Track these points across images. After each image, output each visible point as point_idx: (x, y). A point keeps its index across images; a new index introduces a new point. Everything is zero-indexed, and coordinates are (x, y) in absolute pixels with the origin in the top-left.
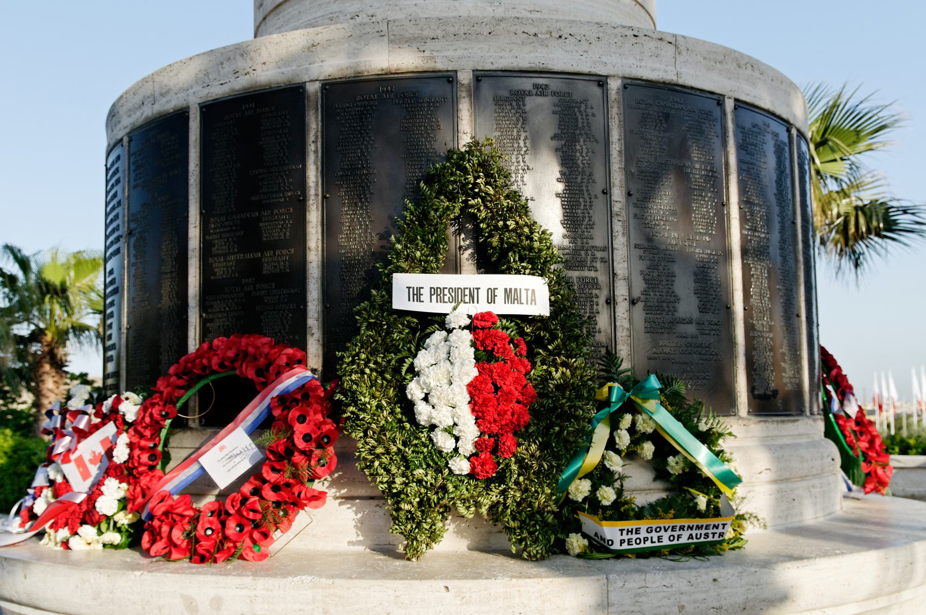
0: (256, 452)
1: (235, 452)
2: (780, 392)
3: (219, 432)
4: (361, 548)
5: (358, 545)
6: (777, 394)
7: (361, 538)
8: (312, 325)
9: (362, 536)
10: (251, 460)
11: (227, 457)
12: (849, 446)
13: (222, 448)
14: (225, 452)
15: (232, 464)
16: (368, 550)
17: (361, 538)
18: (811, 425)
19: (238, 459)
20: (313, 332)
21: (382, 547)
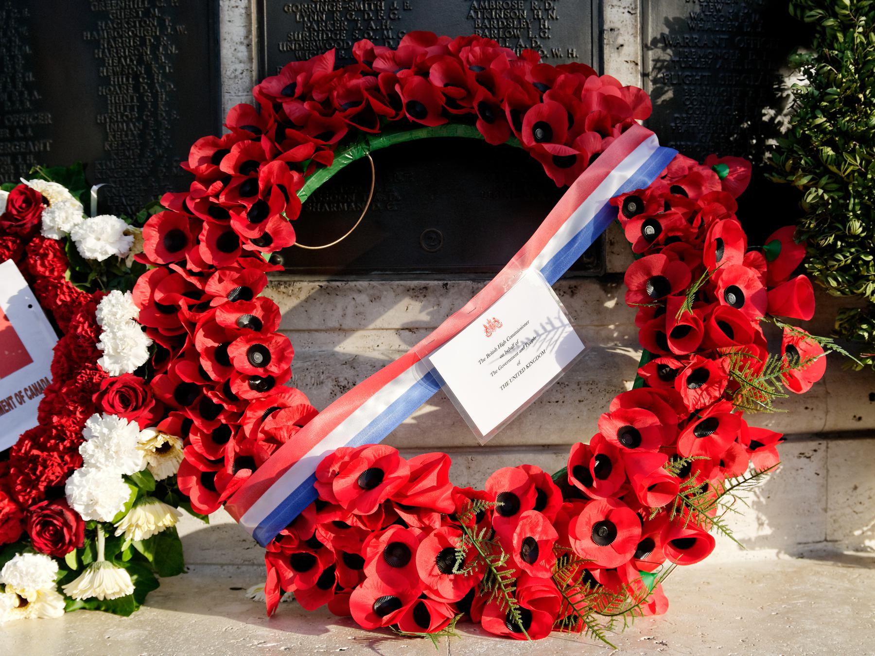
0: (571, 333)
1: (522, 337)
2: (217, 282)
3: (479, 289)
4: (768, 554)
5: (761, 547)
6: (722, 242)
7: (767, 531)
8: (617, 25)
9: (770, 525)
10: (560, 354)
11: (502, 351)
12: (857, 550)
13: (489, 329)
14: (499, 335)
15: (512, 368)
16: (787, 557)
17: (767, 531)
18: (53, 577)
19: (531, 352)
20: (620, 41)
21: (812, 547)
